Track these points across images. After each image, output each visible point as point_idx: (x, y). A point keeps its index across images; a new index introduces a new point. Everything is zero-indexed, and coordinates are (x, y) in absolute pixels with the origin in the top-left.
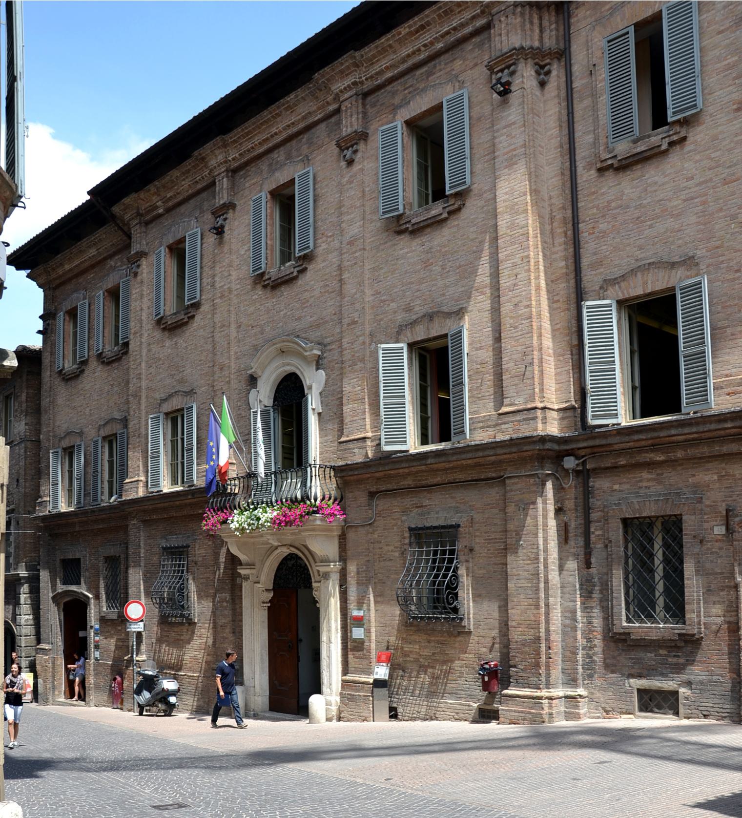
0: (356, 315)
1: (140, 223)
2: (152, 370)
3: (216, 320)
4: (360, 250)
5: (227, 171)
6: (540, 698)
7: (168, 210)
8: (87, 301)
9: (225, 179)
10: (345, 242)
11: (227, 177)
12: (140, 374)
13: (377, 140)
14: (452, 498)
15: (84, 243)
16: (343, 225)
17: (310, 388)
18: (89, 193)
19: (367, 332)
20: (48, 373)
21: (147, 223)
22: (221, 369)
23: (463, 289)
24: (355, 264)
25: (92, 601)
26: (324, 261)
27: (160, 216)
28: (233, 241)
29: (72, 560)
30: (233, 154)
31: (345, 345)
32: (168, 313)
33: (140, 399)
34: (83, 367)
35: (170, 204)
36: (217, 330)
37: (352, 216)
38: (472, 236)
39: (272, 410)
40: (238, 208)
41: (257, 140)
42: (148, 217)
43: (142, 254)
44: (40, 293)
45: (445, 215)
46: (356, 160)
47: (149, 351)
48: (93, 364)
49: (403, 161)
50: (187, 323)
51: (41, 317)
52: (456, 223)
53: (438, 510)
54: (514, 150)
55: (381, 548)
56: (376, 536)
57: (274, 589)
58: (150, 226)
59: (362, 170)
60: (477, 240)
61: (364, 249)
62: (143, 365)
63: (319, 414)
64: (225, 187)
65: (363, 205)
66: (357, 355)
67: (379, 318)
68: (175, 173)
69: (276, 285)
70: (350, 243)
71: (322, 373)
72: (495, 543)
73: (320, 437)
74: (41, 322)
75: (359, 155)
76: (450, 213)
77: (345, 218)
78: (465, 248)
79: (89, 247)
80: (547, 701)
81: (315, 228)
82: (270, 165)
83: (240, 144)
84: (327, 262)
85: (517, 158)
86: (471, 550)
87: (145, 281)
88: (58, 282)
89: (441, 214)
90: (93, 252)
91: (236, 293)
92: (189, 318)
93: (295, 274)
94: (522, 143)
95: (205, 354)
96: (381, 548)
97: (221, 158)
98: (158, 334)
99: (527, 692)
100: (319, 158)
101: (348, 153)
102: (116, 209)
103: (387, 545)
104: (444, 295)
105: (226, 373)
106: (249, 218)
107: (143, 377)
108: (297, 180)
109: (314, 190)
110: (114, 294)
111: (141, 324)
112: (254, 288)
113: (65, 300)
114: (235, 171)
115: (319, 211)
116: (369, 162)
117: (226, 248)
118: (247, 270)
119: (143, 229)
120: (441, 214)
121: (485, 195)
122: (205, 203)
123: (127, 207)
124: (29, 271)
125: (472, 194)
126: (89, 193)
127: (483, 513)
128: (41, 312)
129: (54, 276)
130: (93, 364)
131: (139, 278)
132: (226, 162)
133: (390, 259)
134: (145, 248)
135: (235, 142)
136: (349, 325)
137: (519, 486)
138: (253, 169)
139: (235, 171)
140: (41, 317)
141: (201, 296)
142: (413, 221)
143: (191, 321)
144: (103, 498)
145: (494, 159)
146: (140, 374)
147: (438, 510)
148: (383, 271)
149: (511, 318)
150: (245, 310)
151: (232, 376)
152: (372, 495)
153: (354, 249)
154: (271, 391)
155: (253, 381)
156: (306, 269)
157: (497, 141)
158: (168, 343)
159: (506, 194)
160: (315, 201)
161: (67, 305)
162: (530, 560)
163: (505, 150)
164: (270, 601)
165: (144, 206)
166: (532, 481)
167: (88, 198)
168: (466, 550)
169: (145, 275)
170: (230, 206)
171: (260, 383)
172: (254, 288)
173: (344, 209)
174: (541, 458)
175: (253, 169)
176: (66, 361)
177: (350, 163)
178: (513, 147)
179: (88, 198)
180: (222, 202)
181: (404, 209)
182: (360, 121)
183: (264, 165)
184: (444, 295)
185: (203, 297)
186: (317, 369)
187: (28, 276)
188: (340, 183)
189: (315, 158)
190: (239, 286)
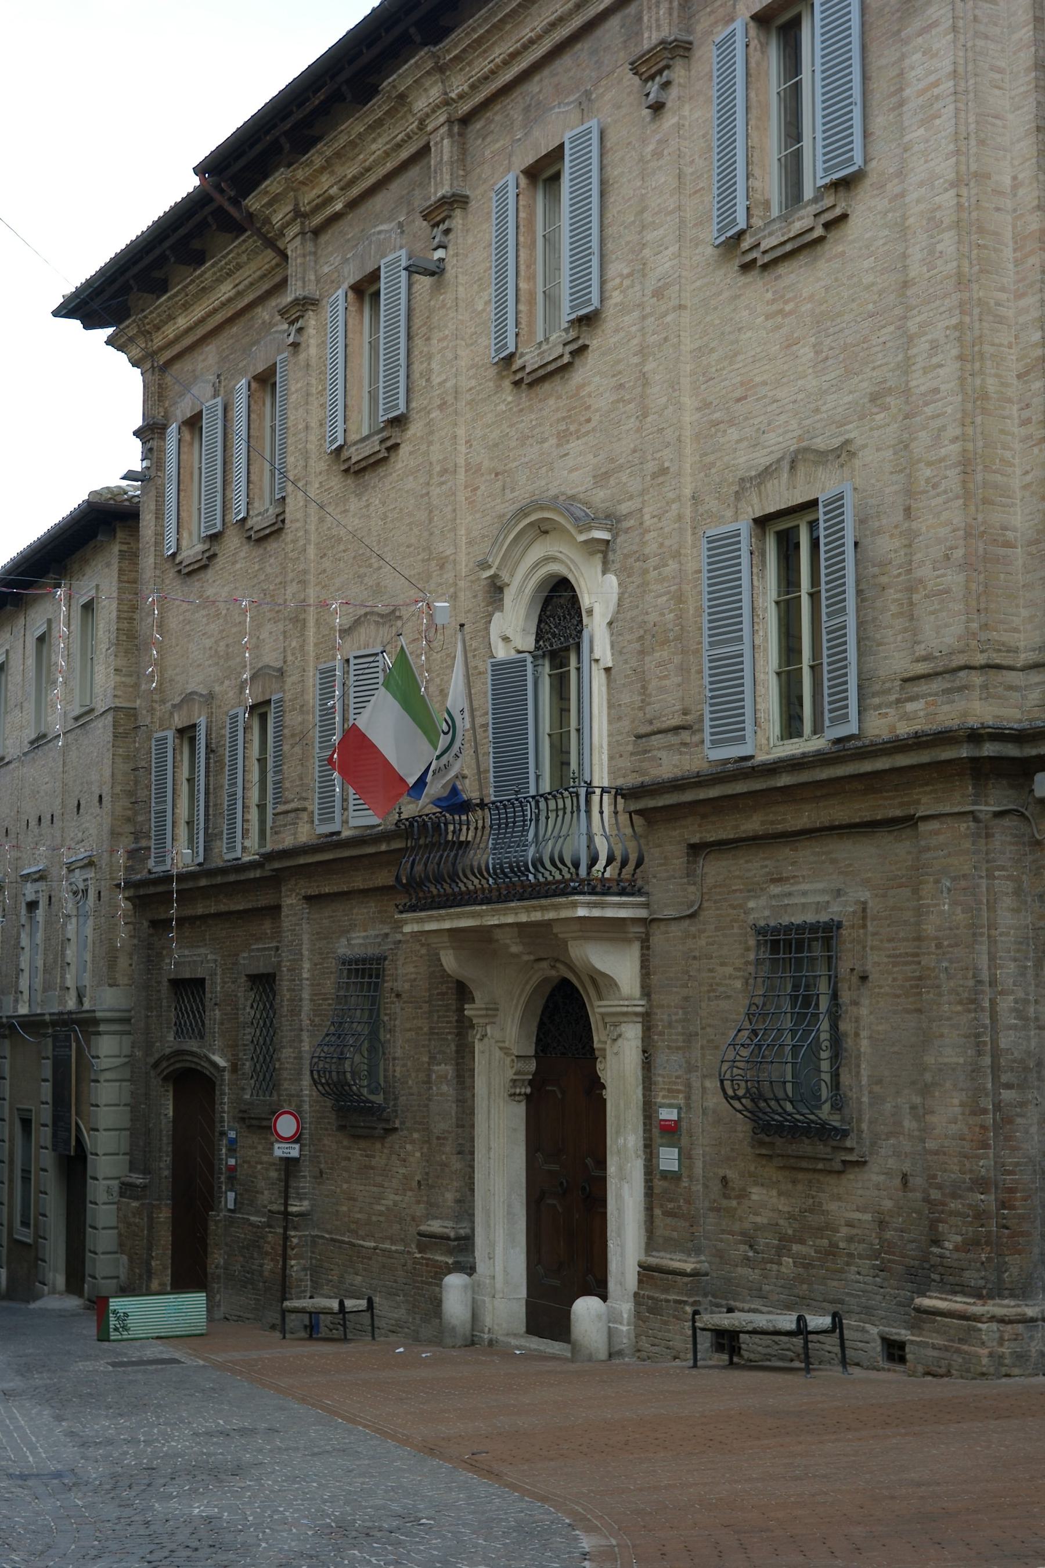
0: (667, 454)
1: (303, 233)
2: (327, 563)
3: (434, 458)
4: (674, 309)
5: (449, 122)
6: (977, 1318)
7: (353, 205)
8: (219, 399)
9: (445, 141)
10: (648, 292)
11: (450, 134)
12: (305, 572)
13: (707, 55)
14: (833, 861)
15: (208, 271)
16: (647, 252)
17: (590, 612)
18: (198, 170)
19: (688, 492)
20: (151, 560)
21: (317, 232)
22: (442, 567)
23: (850, 398)
24: (666, 339)
25: (227, 1076)
26: (617, 331)
27: (337, 217)
28: (462, 279)
29: (191, 980)
30: (458, 84)
31: (648, 521)
32: (353, 437)
33: (304, 626)
34: (216, 548)
35: (355, 191)
36: (435, 480)
37: (661, 231)
38: (868, 279)
39: (530, 659)
40: (473, 205)
41: (500, 51)
42: (317, 220)
43: (306, 304)
44: (134, 378)
45: (819, 232)
46: (669, 105)
47: (321, 520)
48: (233, 541)
49: (748, 109)
50: (385, 459)
51: (137, 433)
52: (840, 249)
53: (809, 889)
54: (936, 84)
55: (711, 970)
56: (703, 942)
57: (536, 1056)
58: (324, 238)
59: (679, 126)
60: (875, 288)
61: (681, 307)
62: (311, 551)
63: (608, 670)
64: (445, 158)
65: (679, 208)
66: (667, 543)
67: (711, 458)
68: (353, 127)
69: (534, 380)
70: (658, 294)
71: (612, 579)
72: (906, 963)
73: (610, 722)
74: (137, 443)
75: (674, 92)
76: (827, 226)
77: (650, 236)
78: (854, 305)
79: (220, 281)
80: (994, 1326)
81: (602, 256)
82: (527, 109)
83: (469, 64)
84: (622, 334)
85: (940, 104)
86: (864, 978)
87: (313, 362)
88: (168, 354)
89: (812, 229)
90: (226, 290)
91: (469, 397)
92: (388, 449)
93: (566, 359)
94: (950, 68)
95: (416, 530)
96: (711, 970)
97: (435, 93)
98: (336, 482)
99: (958, 1303)
100: (608, 97)
101: (653, 87)
102: (254, 203)
103: (723, 964)
104: (817, 410)
105: (449, 576)
106: (488, 231)
107: (311, 578)
108: (567, 147)
109: (602, 168)
110: (266, 381)
111: (307, 459)
112: (499, 388)
113: (182, 395)
114: (465, 121)
115: (612, 212)
116: (693, 110)
117: (448, 297)
118: (487, 349)
119: (310, 246)
120: (812, 229)
121: (889, 186)
122: (416, 192)
123: (273, 198)
124: (110, 331)
125: (867, 182)
126: (198, 170)
127: (884, 896)
128: (138, 422)
129: (158, 341)
130: (233, 541)
131: (302, 356)
132: (447, 102)
133: (728, 329)
134: (311, 290)
135: (457, 58)
136: (654, 475)
137: (941, 838)
138: (496, 115)
139: (465, 121)
140: (137, 433)
141: (408, 402)
142: (764, 246)
143: (393, 454)
144: (247, 843)
145: (901, 104)
146: (305, 572)
147: (809, 889)
148: (715, 356)
149: (929, 464)
150: (484, 437)
151: (462, 584)
152: (695, 850)
153: (663, 308)
154: (527, 616)
155: (496, 589)
156: (584, 348)
157: (907, 62)
158: (354, 504)
159: (921, 184)
160: (602, 194)
161: (184, 409)
162: (960, 1003)
163: (921, 85)
164: (531, 1083)
165: (309, 197)
166: (963, 826)
167: (196, 181)
168: (854, 979)
169: (313, 351)
170: (456, 202)
171: (509, 595)
172: (499, 388)
173: (647, 217)
174: (981, 772)
175: (497, 118)
176: (185, 534)
177: (657, 108)
178: (932, 78)
179: (196, 181)
180: (439, 194)
181: (749, 216)
182: (675, 14)
183: (514, 107)
184: (817, 410)
185: (414, 405)
186: (604, 573)
187: (109, 342)
188: (641, 159)
189: (602, 95)
190: (473, 383)
